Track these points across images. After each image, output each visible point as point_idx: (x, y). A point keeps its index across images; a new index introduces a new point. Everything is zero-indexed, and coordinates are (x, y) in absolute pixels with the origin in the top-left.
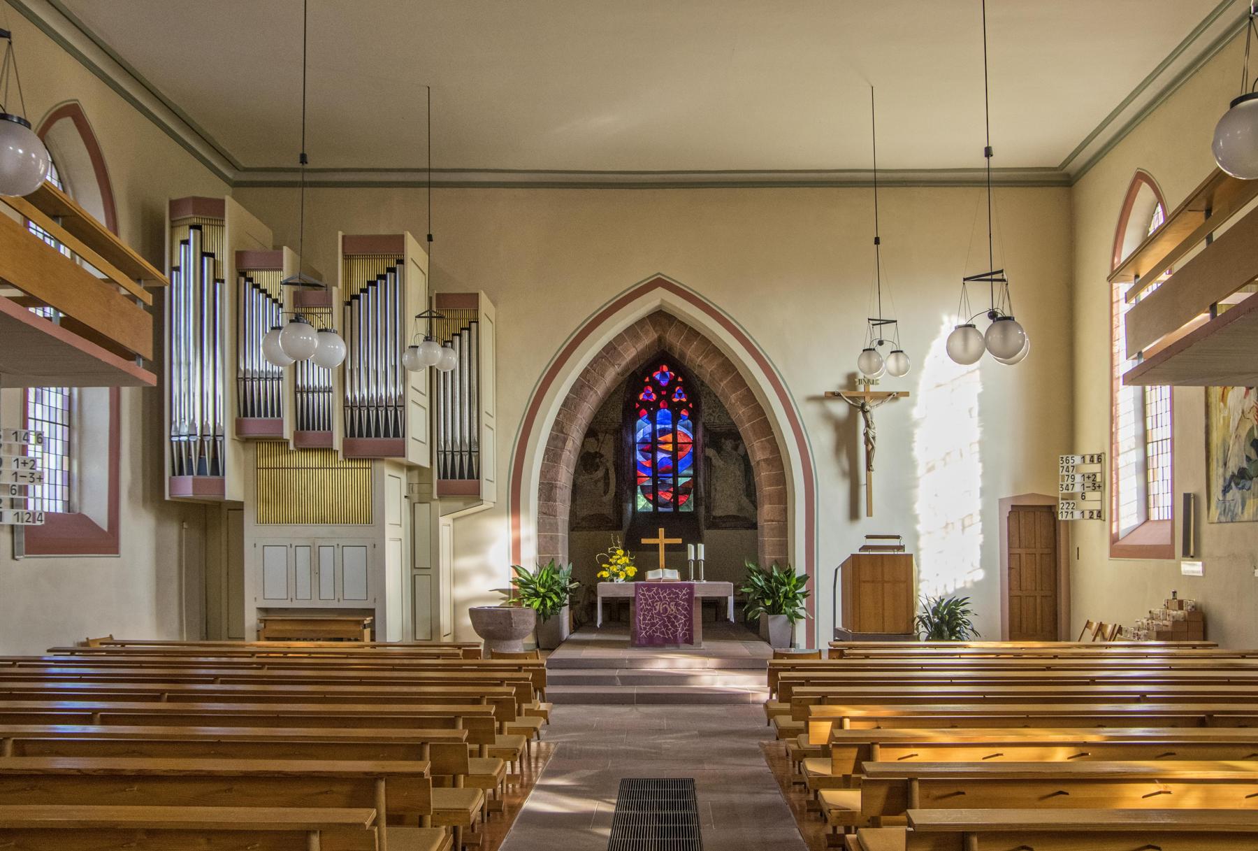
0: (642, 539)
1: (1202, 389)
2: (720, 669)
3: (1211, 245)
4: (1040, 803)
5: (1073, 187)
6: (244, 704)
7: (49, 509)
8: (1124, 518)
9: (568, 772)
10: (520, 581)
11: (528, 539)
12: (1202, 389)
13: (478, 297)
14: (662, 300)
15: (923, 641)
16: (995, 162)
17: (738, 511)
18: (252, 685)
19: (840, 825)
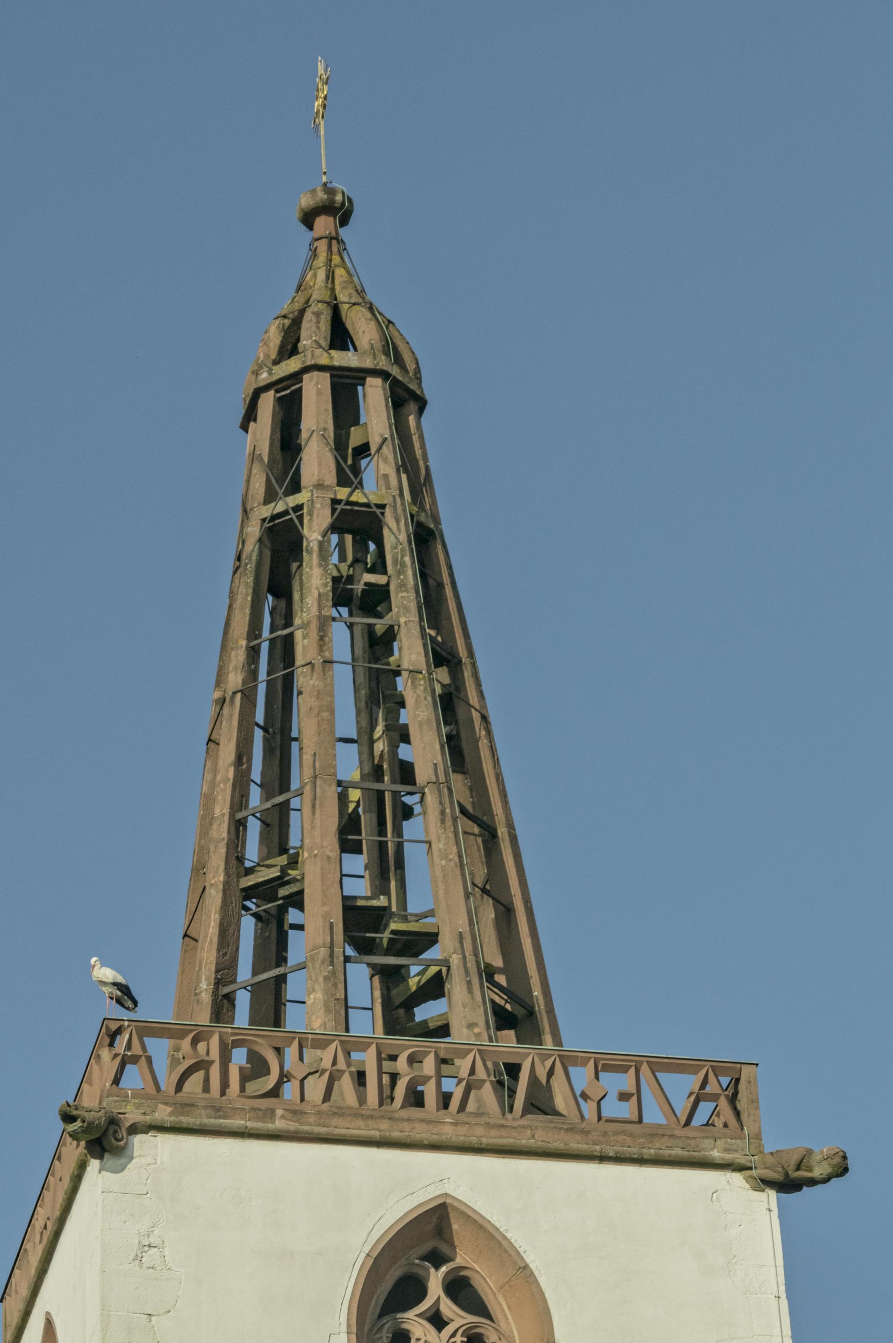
0: (350, 536)
1: (292, 812)
2: (233, 992)
3: (254, 723)
4: (282, 1054)
5: (341, 1080)
6: (536, 1116)
7: (292, 809)
8: (302, 967)
9: (482, 828)
10: (413, 683)
11: (332, 358)
12: (292, 812)
13: (625, 1093)
14: (437, 1111)
15: (358, 623)
16: (292, 933)
17: (318, 698)
18: (458, 1104)
19: (173, 1096)
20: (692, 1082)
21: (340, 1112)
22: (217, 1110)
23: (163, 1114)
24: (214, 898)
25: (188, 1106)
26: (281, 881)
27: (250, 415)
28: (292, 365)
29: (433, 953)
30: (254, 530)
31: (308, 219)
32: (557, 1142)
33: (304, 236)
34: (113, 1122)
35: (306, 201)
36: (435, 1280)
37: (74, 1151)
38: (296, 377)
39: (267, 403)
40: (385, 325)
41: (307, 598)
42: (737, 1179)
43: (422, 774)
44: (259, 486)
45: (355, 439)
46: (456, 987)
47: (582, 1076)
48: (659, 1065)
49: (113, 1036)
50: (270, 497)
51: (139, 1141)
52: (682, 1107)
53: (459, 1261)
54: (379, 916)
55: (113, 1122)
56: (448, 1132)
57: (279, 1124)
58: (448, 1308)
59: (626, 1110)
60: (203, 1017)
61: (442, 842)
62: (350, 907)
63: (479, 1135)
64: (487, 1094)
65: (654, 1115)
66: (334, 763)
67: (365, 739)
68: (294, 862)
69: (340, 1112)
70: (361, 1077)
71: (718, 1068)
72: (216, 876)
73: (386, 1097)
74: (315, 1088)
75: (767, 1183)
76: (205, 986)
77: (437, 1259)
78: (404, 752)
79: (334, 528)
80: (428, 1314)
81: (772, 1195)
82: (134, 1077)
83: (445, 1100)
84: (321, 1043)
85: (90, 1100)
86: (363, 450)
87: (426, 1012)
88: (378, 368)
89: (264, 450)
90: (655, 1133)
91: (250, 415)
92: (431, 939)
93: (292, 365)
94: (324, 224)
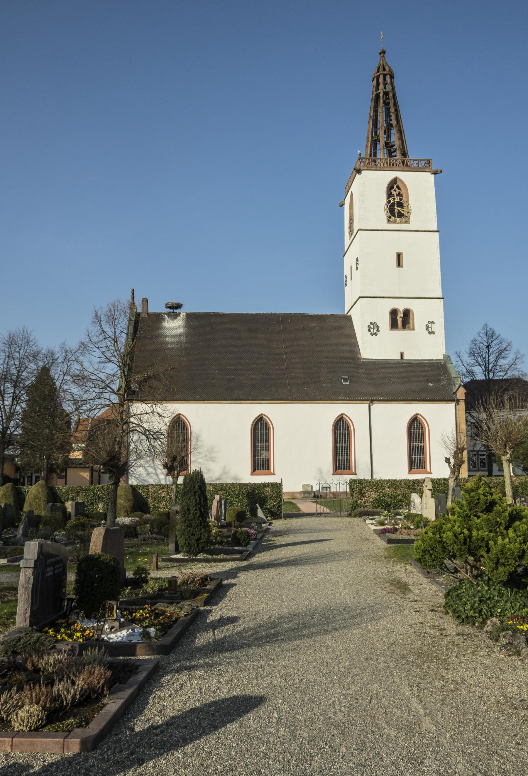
1: (377, 477)
20: (424, 162)
21: (385, 167)
22: (371, 167)
23: (365, 168)
24: (370, 141)
25: (368, 167)
26: (377, 139)
27: (373, 80)
28: (378, 74)
29: (395, 147)
30: (374, 95)
31: (380, 54)
32: (409, 169)
33: (380, 56)
34: (360, 169)
35: (380, 51)
36: (395, 186)
37: (354, 173)
38: (379, 75)
39: (375, 79)
40: (390, 68)
41: (174, 653)
42: (429, 173)
43: (394, 125)
44: (374, 90)
45: (386, 82)
46: (398, 151)
47: (412, 162)
48: (421, 160)
49: (359, 159)
50: (376, 91)
51: (363, 172)
52: (423, 165)
53: (398, 184)
54: (388, 143)
55: (360, 169)
56: (397, 169)
57: (378, 169)
58: (397, 189)
59: (417, 166)
60: (368, 157)
61: (505, 458)
62: (385, 142)
63: (400, 169)
64: (401, 164)
65: (420, 166)
66: (421, 444)
67: (386, 121)
68: (378, 136)
69: (385, 167)
70: (387, 163)
71: (427, 160)
72: (370, 139)
73: (390, 165)
74: (382, 164)
75: (432, 174)
76: (369, 152)
77: (395, 184)
78: (391, 122)
79: (384, 95)
80: (423, 470)
81: (433, 175)
82: (362, 164)
83: (397, 164)
84: (383, 159)
85: (357, 167)
86: (387, 84)
87: (393, 154)
88: (168, 424)
89: (375, 85)
90: (420, 168)
91: (373, 80)
92: (394, 145)
93: (378, 74)
94: (382, 54)
